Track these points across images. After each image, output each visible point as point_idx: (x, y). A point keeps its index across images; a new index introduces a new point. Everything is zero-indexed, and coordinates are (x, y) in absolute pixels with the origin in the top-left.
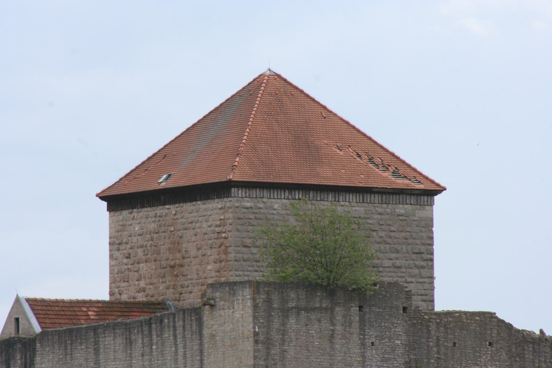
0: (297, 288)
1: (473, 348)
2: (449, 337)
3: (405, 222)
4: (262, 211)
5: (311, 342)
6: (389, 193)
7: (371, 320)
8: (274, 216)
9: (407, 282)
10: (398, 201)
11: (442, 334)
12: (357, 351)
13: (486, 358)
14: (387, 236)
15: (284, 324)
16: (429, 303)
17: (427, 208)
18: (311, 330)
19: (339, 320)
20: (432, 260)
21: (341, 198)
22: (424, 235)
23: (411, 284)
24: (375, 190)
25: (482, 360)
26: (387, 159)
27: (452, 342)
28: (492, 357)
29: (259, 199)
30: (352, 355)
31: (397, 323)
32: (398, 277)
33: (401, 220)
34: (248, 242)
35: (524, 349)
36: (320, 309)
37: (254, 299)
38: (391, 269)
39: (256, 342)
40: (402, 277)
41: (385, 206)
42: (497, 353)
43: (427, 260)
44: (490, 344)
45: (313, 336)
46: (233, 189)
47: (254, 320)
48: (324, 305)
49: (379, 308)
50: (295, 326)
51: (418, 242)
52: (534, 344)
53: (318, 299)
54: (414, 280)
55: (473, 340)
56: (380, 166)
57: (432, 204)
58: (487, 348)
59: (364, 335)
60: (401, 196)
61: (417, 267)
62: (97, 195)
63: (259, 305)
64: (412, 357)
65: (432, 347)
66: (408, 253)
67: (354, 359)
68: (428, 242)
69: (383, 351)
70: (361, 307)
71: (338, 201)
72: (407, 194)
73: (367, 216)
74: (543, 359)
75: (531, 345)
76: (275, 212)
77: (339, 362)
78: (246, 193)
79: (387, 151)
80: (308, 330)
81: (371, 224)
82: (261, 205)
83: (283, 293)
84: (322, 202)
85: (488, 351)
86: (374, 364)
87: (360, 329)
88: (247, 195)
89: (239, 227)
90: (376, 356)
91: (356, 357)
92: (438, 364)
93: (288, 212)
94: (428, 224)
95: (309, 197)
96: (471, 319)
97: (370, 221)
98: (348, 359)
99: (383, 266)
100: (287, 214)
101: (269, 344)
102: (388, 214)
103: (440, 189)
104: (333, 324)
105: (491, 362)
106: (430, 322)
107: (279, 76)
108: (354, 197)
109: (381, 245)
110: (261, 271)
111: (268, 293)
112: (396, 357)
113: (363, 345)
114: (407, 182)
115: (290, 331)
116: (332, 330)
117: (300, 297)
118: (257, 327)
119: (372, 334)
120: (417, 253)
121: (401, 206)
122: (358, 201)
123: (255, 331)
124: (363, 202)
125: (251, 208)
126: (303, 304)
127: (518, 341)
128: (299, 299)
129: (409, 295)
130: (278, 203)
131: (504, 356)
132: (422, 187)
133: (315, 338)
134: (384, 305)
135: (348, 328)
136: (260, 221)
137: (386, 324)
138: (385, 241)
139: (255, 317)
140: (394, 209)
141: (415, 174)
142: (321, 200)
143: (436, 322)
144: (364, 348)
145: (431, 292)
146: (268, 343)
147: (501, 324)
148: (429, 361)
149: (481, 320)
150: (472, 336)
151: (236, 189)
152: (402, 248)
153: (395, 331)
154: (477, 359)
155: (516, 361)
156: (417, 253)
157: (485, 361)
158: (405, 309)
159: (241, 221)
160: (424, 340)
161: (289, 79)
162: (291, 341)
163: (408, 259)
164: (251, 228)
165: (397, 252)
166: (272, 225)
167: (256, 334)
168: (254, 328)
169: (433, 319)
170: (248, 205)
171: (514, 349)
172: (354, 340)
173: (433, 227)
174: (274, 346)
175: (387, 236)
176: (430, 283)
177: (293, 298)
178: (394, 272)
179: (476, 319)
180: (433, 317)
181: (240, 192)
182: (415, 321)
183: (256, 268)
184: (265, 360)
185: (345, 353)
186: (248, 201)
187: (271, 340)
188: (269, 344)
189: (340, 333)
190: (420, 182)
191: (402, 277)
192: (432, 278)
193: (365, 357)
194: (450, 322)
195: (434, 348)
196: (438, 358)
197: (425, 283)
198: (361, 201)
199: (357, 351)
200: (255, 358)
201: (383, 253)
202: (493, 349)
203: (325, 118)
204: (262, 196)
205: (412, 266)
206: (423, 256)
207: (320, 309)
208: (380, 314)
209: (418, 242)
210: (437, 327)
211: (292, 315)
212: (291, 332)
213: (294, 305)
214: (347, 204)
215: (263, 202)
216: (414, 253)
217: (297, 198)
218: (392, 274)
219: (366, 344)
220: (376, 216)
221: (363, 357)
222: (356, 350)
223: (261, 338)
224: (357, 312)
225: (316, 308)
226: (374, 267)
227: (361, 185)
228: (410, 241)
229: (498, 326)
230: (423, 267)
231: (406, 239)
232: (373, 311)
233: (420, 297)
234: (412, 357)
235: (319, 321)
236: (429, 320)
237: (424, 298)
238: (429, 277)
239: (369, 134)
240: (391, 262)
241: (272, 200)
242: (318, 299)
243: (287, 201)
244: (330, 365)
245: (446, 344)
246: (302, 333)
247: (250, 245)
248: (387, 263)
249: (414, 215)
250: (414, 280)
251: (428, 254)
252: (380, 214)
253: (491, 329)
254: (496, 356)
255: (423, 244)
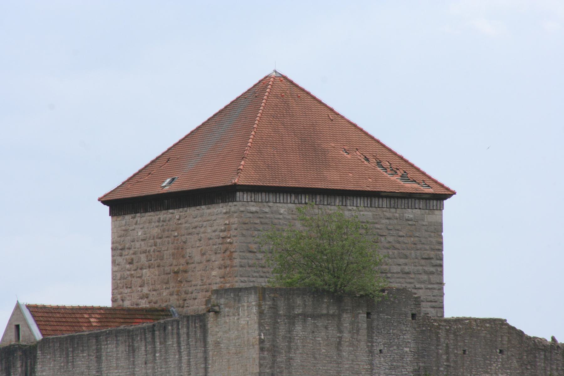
0: (304, 294)
1: (484, 355)
2: (459, 344)
3: (414, 227)
4: (268, 216)
5: (318, 350)
6: (398, 198)
7: (379, 327)
8: (280, 221)
9: (416, 289)
10: (406, 205)
11: (452, 342)
12: (364, 358)
13: (497, 366)
14: (395, 241)
15: (290, 331)
16: (438, 310)
17: (437, 212)
18: (318, 337)
19: (346, 327)
20: (441, 266)
21: (348, 202)
22: (433, 240)
23: (420, 291)
24: (383, 194)
25: (492, 367)
26: (396, 163)
27: (462, 349)
28: (503, 365)
29: (265, 204)
30: (360, 363)
31: (406, 330)
32: (406, 283)
33: (410, 225)
34: (254, 247)
35: (536, 357)
36: (327, 315)
37: (259, 306)
38: (399, 275)
39: (262, 349)
40: (410, 283)
41: (393, 210)
42: (508, 360)
43: (436, 266)
44: (501, 352)
45: (320, 343)
46: (238, 193)
47: (259, 327)
48: (331, 312)
49: (387, 315)
50: (301, 333)
51: (427, 247)
52: (545, 352)
53: (325, 306)
54: (423, 286)
55: (483, 347)
56: (389, 170)
57: (441, 209)
58: (498, 356)
59: (372, 342)
60: (410, 200)
61: (426, 272)
62: (99, 200)
63: (265, 312)
64: (421, 364)
65: (442, 355)
66: (416, 258)
67: (361, 366)
68: (437, 247)
69: (392, 359)
70: (368, 314)
71: (346, 205)
72: (415, 198)
73: (375, 221)
74: (555, 367)
75: (542, 353)
76: (281, 217)
77: (347, 370)
78: (251, 197)
79: (395, 154)
80: (315, 337)
81: (379, 229)
82: (267, 210)
83: (289, 299)
84: (329, 206)
85: (499, 358)
86: (382, 372)
87: (368, 336)
88: (253, 199)
89: (244, 232)
90: (384, 364)
91: (363, 365)
92: (447, 372)
93: (295, 216)
94: (438, 229)
95: (316, 202)
96: (482, 326)
97: (378, 226)
98: (355, 367)
99: (391, 271)
100: (293, 219)
101: (275, 351)
102: (397, 219)
103: (450, 193)
104: (341, 332)
105: (502, 370)
106: (440, 329)
107: (285, 78)
108: (362, 202)
109: (389, 251)
110: (267, 277)
111: (274, 300)
112: (404, 365)
113: (371, 352)
114: (416, 186)
115: (296, 338)
116: (339, 337)
117: (306, 303)
118: (262, 334)
119: (380, 342)
120: (426, 259)
121: (410, 210)
122: (366, 205)
123: (260, 339)
124: (371, 207)
125: (257, 212)
126: (309, 310)
127: (529, 348)
128: (305, 305)
129: (418, 301)
130: (284, 208)
131: (515, 364)
132: (431, 191)
133: (322, 345)
134: (392, 312)
135: (356, 335)
136: (265, 226)
137: (394, 331)
138: (394, 247)
139: (260, 324)
140: (403, 214)
141: (424, 178)
142: (328, 205)
143: (446, 329)
144: (372, 356)
145: (440, 298)
146: (274, 350)
147: (511, 331)
148: (438, 369)
149: (492, 327)
150: (482, 343)
151: (241, 193)
152: (411, 254)
153: (404, 338)
154: (487, 366)
155: (528, 369)
156: (426, 259)
157: (496, 369)
158: (413, 316)
159: (247, 225)
160: (433, 348)
161: (296, 81)
162: (297, 348)
163: (417, 264)
164: (256, 233)
165: (406, 257)
166: (278, 230)
167: (261, 341)
168: (260, 335)
169: (443, 326)
170: (254, 209)
171: (525, 357)
172: (362, 347)
173: (442, 232)
174: (280, 353)
175: (395, 241)
176: (439, 289)
177: (300, 305)
178: (403, 278)
179: (486, 326)
180: (443, 324)
181: (245, 196)
182: (424, 328)
183: (262, 274)
184: (271, 368)
185: (353, 361)
186: (253, 206)
187: (277, 347)
188: (275, 351)
189: (347, 340)
190: (429, 186)
191: (410, 283)
192: (441, 284)
193: (373, 364)
194: (460, 329)
195: (443, 356)
196: (447, 366)
197: (434, 289)
198: (369, 206)
199: (364, 358)
200: (261, 365)
201: (392, 258)
202: (504, 356)
203: (332, 120)
204: (267, 200)
205: (421, 272)
206: (433, 261)
207: (327, 315)
208: (389, 320)
209: (427, 247)
210: (447, 334)
211: (298, 322)
212: (297, 340)
213: (300, 311)
214: (355, 208)
215: (269, 206)
216: (423, 258)
217: (303, 202)
218: (401, 280)
219: (374, 352)
220: (384, 221)
221: (371, 364)
222: (363, 357)
223: (267, 345)
224: (365, 319)
225: (323, 315)
226: (382, 273)
227: (369, 189)
228: (419, 246)
229: (508, 333)
230: (432, 273)
231: (415, 244)
232: (381, 318)
233: (429, 304)
234: (421, 364)
235: (326, 328)
236: (438, 327)
237: (434, 304)
238: (438, 283)
239: (377, 137)
240: (399, 267)
241: (278, 205)
242: (325, 306)
243: (294, 205)
244: (337, 373)
245: (456, 352)
246: (308, 341)
247: (255, 251)
248: (396, 269)
249: (423, 220)
250: (423, 286)
251: (437, 259)
252: (388, 219)
253: (502, 336)
254: (507, 364)
255: (432, 250)
